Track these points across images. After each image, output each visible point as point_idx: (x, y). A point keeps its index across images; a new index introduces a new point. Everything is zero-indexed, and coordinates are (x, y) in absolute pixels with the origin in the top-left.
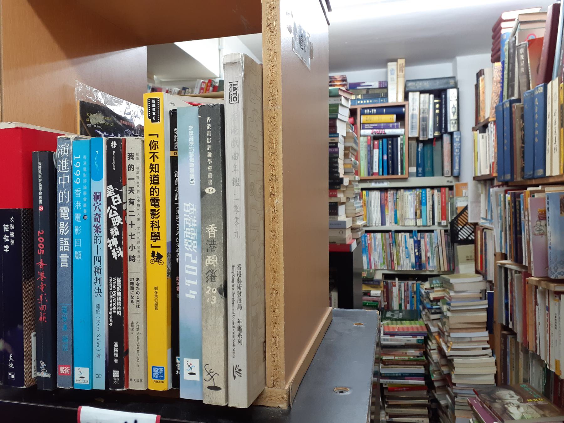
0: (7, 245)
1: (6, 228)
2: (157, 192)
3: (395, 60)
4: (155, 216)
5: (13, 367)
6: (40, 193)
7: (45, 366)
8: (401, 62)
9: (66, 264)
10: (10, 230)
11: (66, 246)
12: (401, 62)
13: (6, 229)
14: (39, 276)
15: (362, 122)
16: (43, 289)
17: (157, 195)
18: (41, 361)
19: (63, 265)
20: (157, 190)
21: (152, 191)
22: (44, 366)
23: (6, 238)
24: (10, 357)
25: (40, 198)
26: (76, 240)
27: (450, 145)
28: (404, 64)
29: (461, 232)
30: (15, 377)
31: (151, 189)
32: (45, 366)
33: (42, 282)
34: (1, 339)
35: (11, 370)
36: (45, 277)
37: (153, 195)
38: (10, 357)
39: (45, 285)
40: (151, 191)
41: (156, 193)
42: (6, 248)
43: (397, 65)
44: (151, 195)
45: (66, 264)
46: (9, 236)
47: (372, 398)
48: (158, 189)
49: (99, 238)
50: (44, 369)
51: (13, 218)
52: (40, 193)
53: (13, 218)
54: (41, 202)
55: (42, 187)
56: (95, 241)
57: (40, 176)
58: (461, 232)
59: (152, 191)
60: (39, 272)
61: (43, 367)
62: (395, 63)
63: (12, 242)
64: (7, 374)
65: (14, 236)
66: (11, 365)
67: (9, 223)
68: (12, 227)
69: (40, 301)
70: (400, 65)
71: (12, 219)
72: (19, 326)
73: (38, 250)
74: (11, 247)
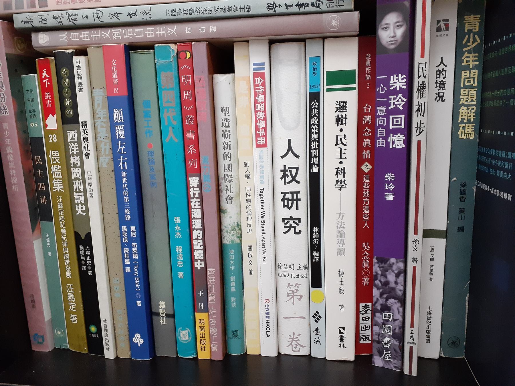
2: (444, 74)
4: (187, 95)
9: (257, 82)
11: (383, 122)
15: (282, 260)
17: (444, 78)
19: (257, 80)
20: (444, 73)
21: (438, 74)
26: (401, 118)
27: (214, 129)
29: (61, 182)
31: (437, 71)
37: (439, 78)
40: (437, 74)
41: (443, 74)
44: (437, 78)
45: (257, 82)
47: (319, 93)
48: (446, 71)
49: (229, 155)
56: (225, 158)
58: (61, 182)
59: (438, 74)
72: (73, 185)
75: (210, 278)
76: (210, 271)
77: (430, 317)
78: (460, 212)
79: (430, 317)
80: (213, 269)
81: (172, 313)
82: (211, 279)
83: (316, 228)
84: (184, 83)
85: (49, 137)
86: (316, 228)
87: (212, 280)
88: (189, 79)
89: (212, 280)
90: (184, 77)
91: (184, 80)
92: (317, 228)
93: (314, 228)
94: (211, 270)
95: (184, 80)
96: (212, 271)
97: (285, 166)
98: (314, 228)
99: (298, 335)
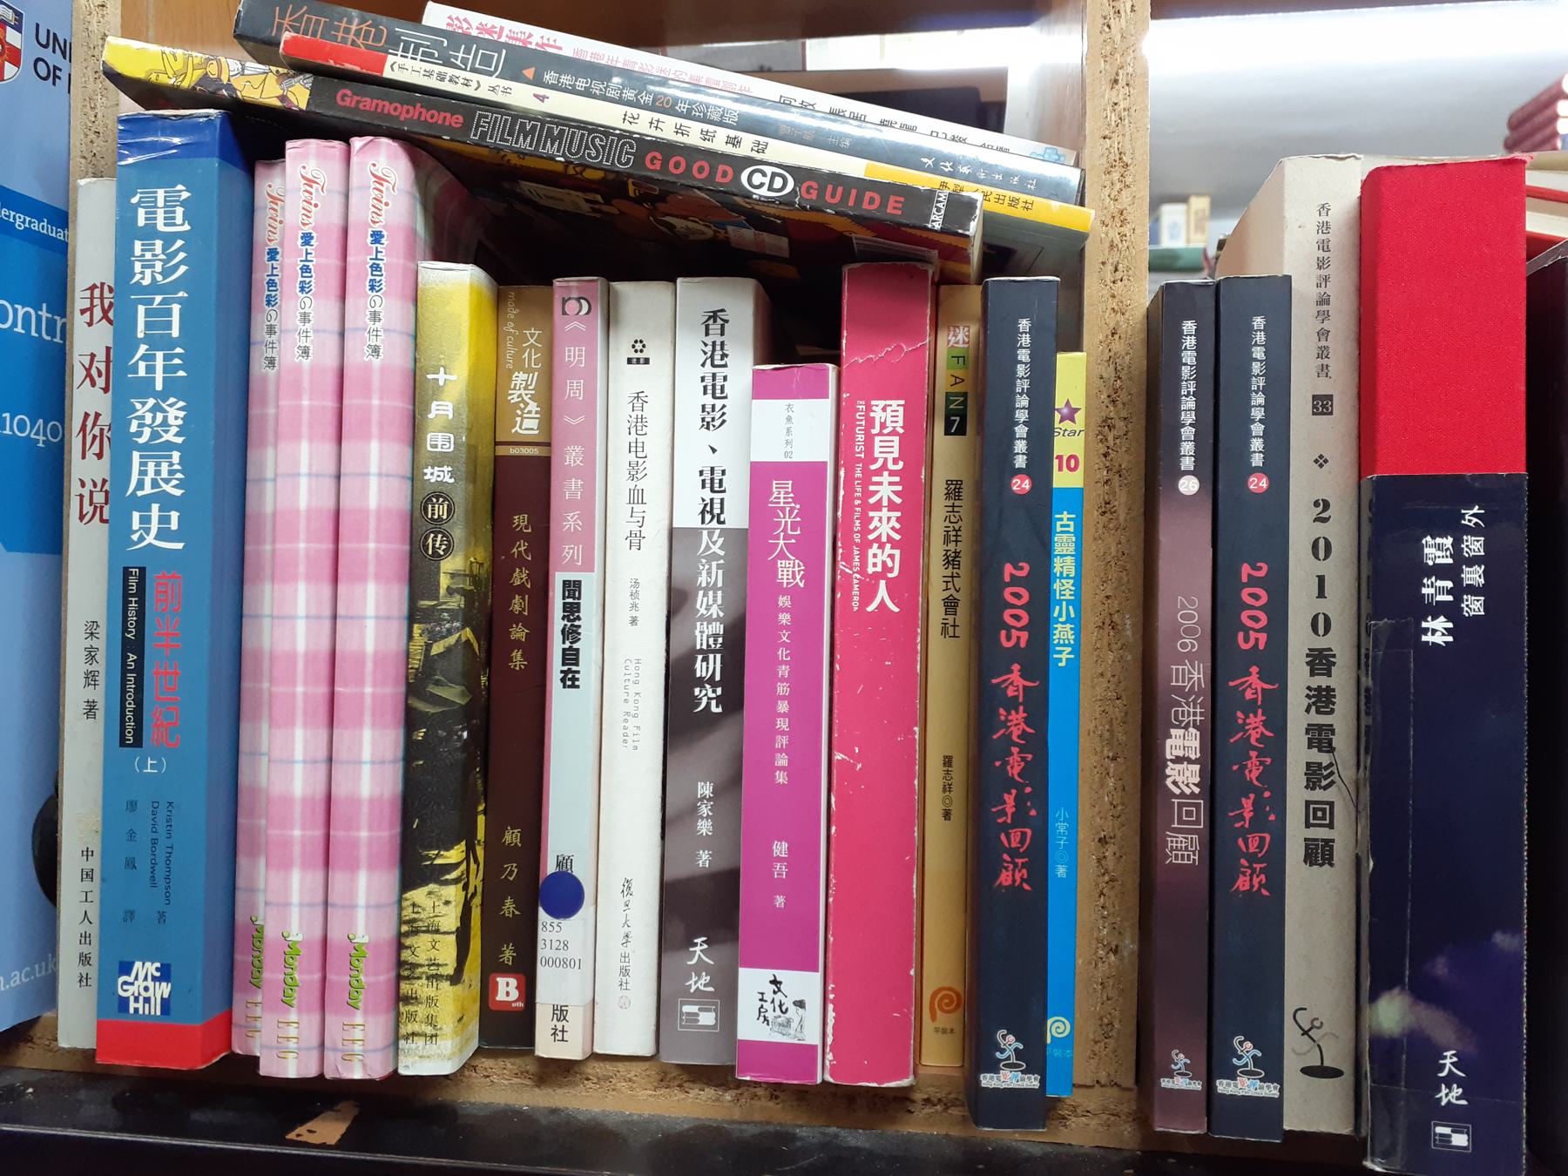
0: (1442, 618)
1: (1436, 550)
3: (1183, 199)
5: (1464, 1102)
6: (1257, 429)
7: (1254, 1057)
8: (1200, 204)
10: (1460, 560)
12: (1200, 204)
13: (1440, 553)
14: (1005, 724)
16: (1255, 774)
18: (1237, 1040)
22: (1250, 1055)
23: (1440, 591)
24: (1448, 1062)
25: (1257, 444)
28: (1207, 213)
30: (1474, 1140)
32: (1254, 1057)
33: (1255, 748)
34: (1396, 991)
35: (1451, 1115)
36: (1267, 733)
38: (1448, 1062)
39: (1269, 760)
42: (1437, 631)
43: (1188, 212)
46: (1457, 581)
50: (1013, 1060)
51: (1476, 510)
52: (1257, 429)
53: (1476, 510)
54: (1257, 460)
55: (1030, 409)
57: (1021, 370)
60: (1239, 714)
61: (1247, 1059)
62: (1181, 208)
63: (1474, 606)
64: (1427, 1131)
65: (1482, 581)
66: (1450, 1095)
67: (1458, 531)
68: (1474, 546)
69: (1241, 817)
70: (1196, 213)
71: (1471, 516)
73: (1003, 633)
74: (1461, 626)
75: (1195, 707)
76: (1190, 673)
77: (959, 538)
78: (944, 790)
79: (959, 538)
80: (1199, 684)
81: (943, 288)
82: (1192, 710)
83: (1426, 631)
84: (570, 363)
85: (12, 975)
86: (1426, 631)
87: (1189, 712)
88: (580, 356)
89: (1189, 712)
90: (570, 351)
91: (569, 356)
92: (1424, 625)
93: (1424, 638)
94: (1196, 676)
95: (569, 356)
96: (1190, 679)
97: (54, 84)
98: (1424, 638)
99: (756, 68)
